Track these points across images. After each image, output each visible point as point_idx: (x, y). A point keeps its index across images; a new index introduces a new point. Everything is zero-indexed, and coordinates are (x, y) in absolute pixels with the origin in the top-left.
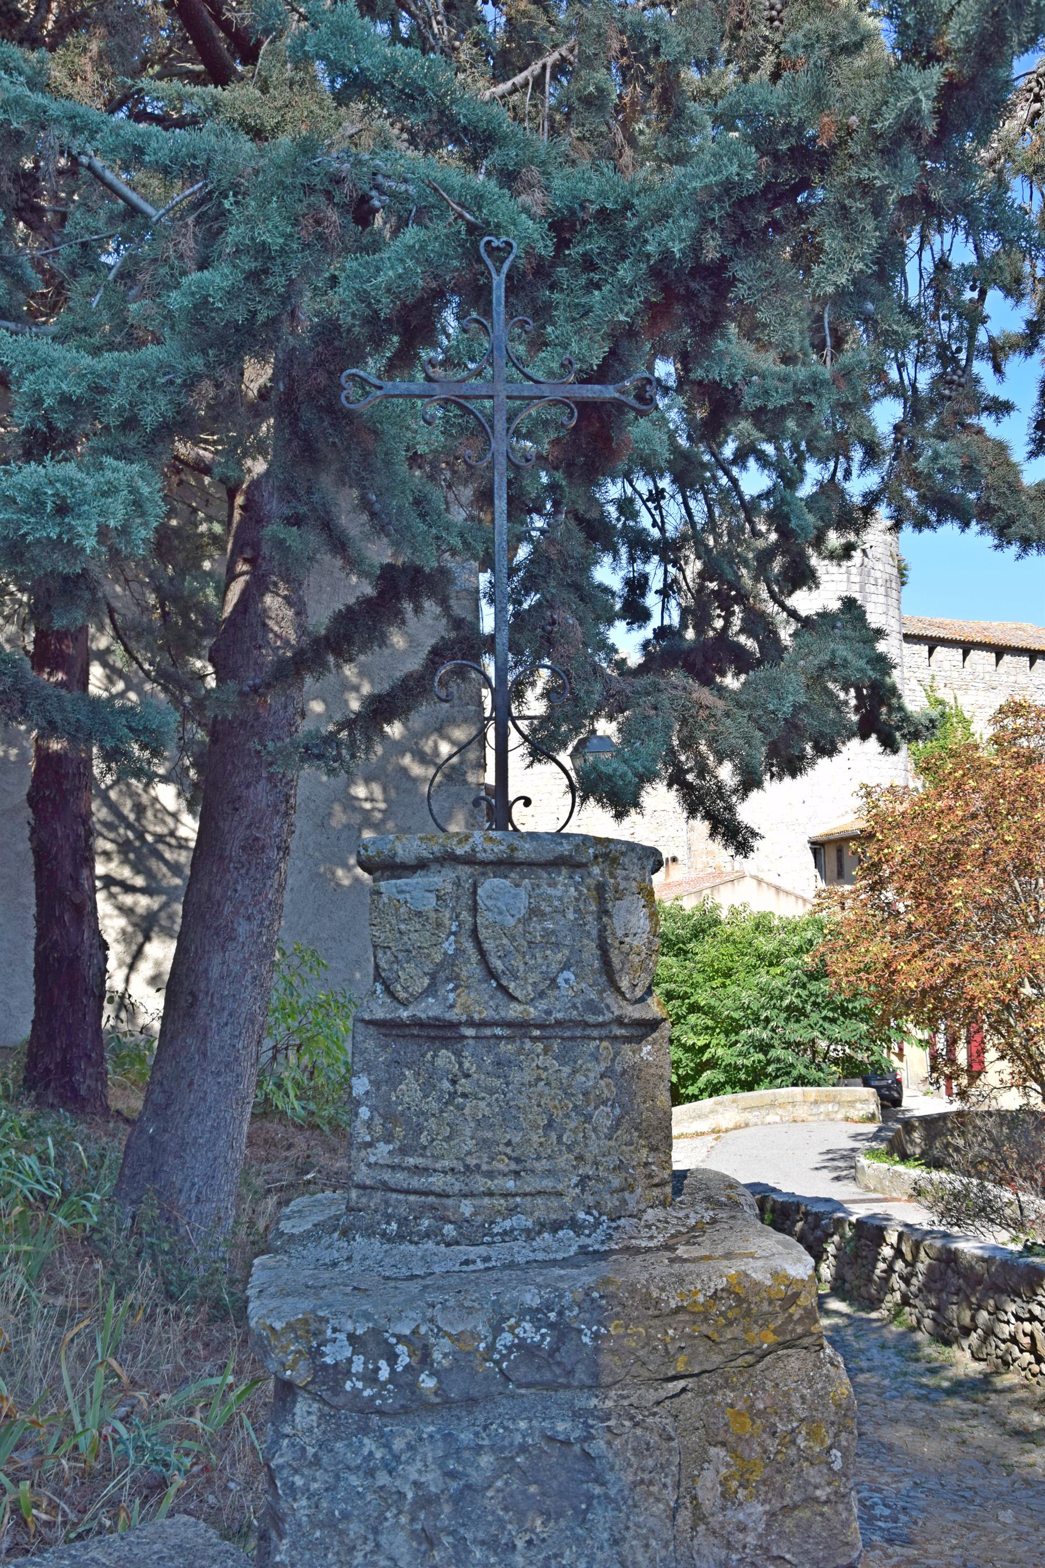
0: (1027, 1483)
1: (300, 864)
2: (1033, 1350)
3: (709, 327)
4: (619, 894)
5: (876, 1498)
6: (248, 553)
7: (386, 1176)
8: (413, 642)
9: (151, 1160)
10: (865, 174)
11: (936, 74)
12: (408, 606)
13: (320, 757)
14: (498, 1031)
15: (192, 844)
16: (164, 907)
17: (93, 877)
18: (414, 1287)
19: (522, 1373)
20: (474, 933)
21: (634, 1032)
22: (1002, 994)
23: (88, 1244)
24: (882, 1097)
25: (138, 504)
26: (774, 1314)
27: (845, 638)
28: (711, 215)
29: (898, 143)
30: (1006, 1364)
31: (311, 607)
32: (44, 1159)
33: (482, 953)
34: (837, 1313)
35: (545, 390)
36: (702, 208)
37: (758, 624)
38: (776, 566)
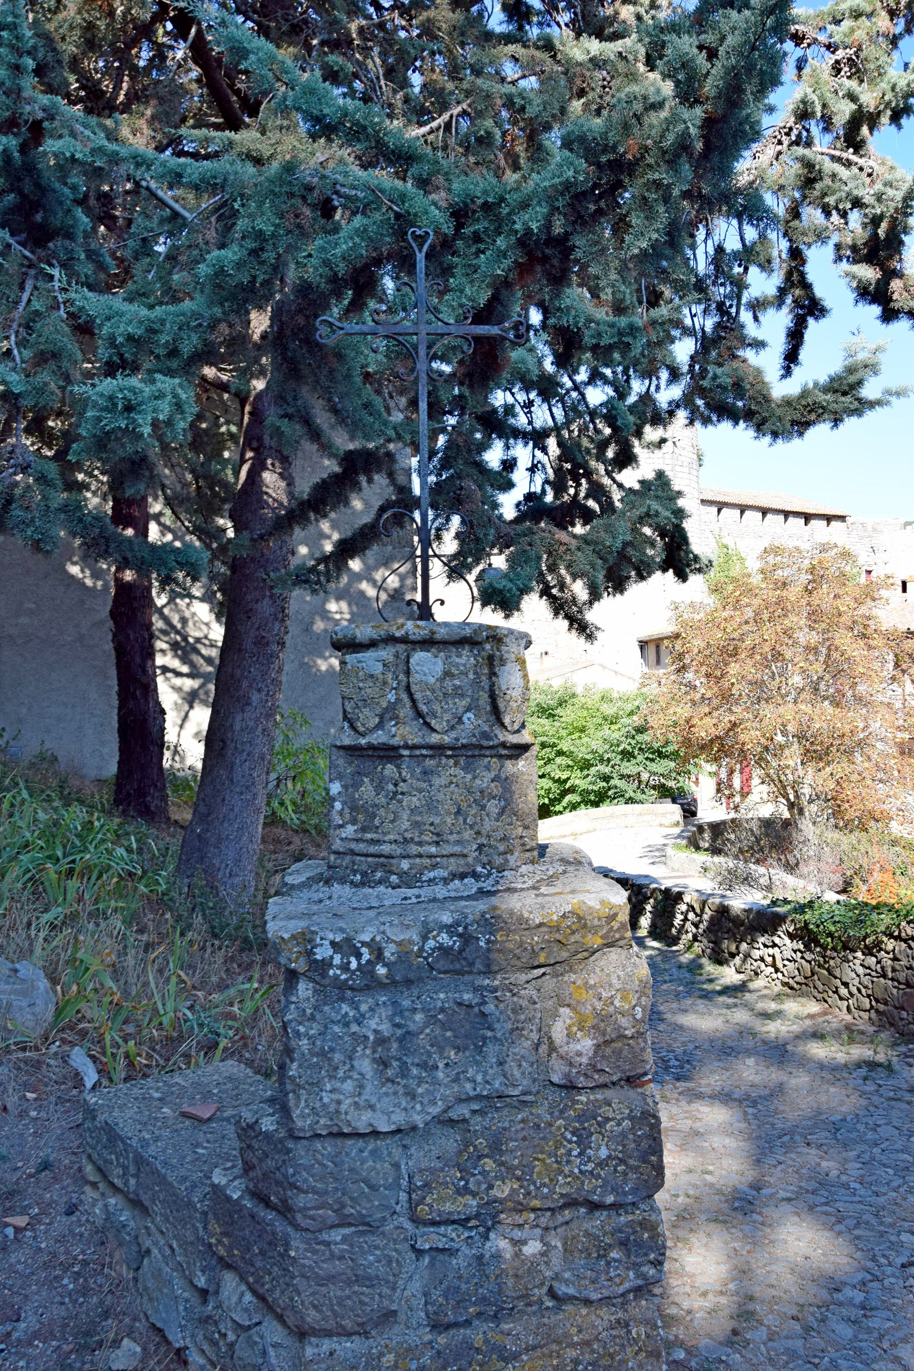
0: (765, 1042)
1: (292, 657)
2: (774, 965)
3: (559, 280)
4: (503, 662)
5: (671, 1055)
6: (255, 444)
7: (353, 846)
8: (366, 503)
9: (199, 850)
10: (656, 176)
11: (698, 111)
12: (363, 479)
13: (306, 582)
14: (424, 752)
15: (220, 644)
16: (202, 686)
17: (154, 667)
18: (372, 913)
19: (442, 965)
20: (408, 688)
21: (513, 752)
22: (763, 741)
23: (161, 903)
24: (684, 811)
25: (178, 406)
26: (601, 926)
27: (657, 497)
28: (557, 204)
29: (677, 156)
30: (757, 974)
31: (297, 481)
32: (129, 850)
33: (413, 701)
34: (653, 948)
35: (452, 329)
36: (551, 200)
37: (597, 491)
38: (610, 454)
